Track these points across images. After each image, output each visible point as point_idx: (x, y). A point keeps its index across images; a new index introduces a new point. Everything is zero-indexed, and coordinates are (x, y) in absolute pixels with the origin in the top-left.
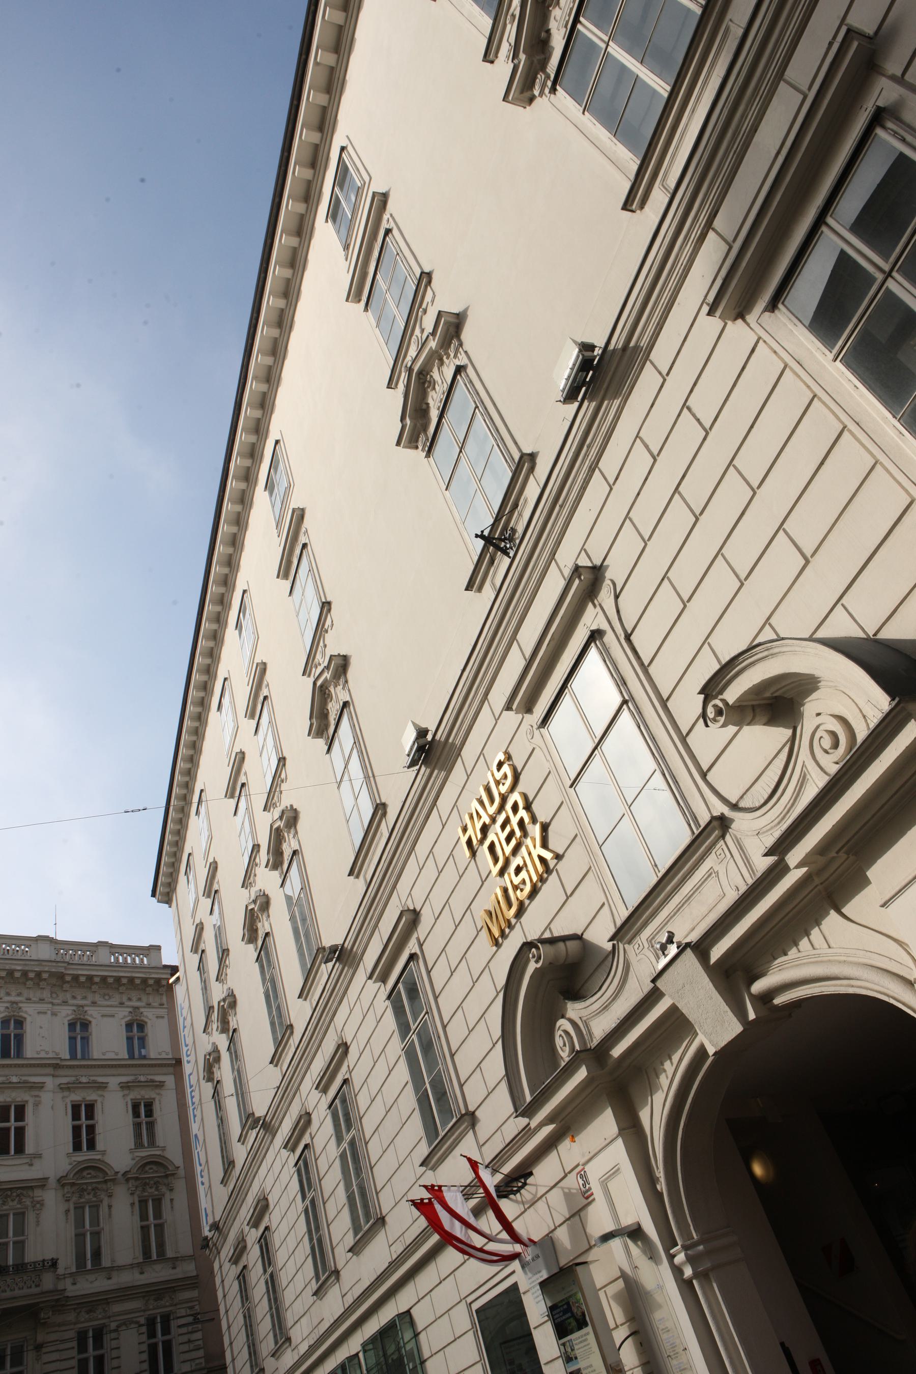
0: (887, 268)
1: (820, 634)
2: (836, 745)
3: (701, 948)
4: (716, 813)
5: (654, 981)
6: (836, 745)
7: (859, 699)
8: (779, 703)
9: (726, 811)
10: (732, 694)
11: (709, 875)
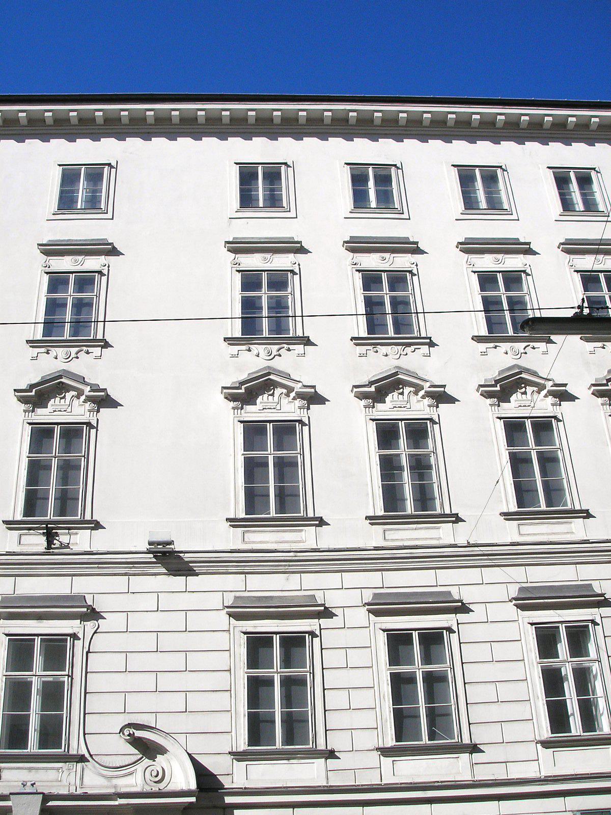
0: (69, 297)
1: (198, 758)
2: (156, 776)
3: (46, 798)
4: (80, 753)
5: (11, 794)
6: (156, 776)
7: (183, 778)
8: (149, 750)
9: (87, 755)
10: (138, 734)
11: (58, 769)
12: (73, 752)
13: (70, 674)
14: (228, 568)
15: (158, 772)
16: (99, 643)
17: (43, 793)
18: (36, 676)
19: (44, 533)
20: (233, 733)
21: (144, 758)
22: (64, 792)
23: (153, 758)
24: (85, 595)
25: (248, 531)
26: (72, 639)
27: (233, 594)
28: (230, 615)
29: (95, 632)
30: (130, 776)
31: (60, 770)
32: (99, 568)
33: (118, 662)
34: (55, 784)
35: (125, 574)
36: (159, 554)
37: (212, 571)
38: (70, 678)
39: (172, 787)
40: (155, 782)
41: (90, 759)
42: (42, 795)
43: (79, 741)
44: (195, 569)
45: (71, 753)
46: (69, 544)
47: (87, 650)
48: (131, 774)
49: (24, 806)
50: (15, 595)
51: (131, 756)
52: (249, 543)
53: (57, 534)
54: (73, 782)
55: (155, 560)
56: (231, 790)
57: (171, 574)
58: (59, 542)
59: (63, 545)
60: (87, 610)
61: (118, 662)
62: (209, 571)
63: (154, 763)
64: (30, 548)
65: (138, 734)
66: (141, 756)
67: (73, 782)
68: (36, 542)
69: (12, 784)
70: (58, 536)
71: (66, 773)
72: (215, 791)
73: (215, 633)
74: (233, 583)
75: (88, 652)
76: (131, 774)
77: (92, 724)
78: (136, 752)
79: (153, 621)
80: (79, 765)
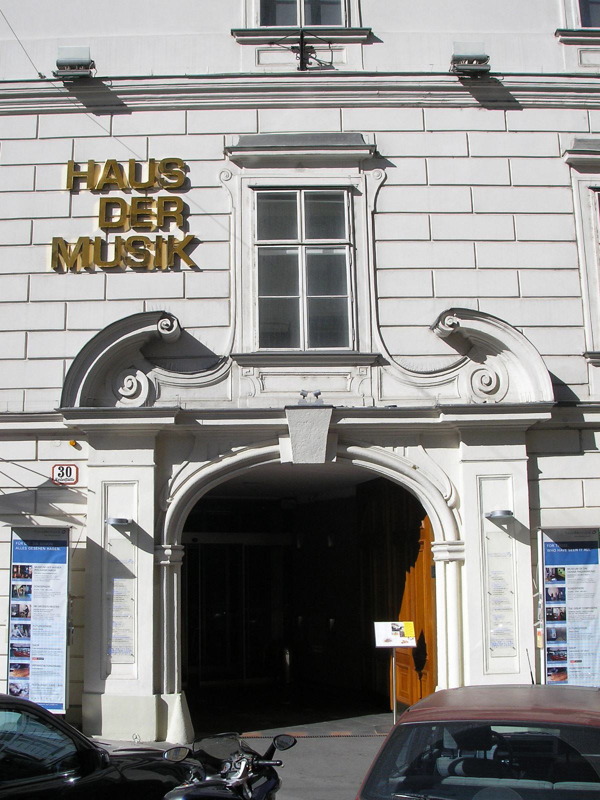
3: (338, 413)
5: (286, 407)
8: (471, 346)
9: (385, 356)
11: (345, 375)
12: (365, 349)
13: (352, 243)
14: (563, 100)
15: (490, 378)
16: (389, 199)
17: (331, 407)
18: (302, 245)
19: (293, 48)
20: (587, 328)
21: (469, 359)
22: (358, 405)
23: (481, 359)
24: (362, 133)
25: (586, 50)
26: (350, 194)
27: (573, 136)
28: (571, 164)
29: (382, 185)
30: (451, 384)
31: (349, 377)
32: (379, 95)
33: (417, 227)
34: (342, 394)
35: (417, 105)
36: (466, 77)
37: (541, 103)
38: (352, 248)
39: (510, 400)
40: (488, 393)
41: (389, 360)
42: (331, 410)
43: (371, 335)
44: (517, 99)
45: (361, 351)
46: (331, 63)
47: (373, 209)
48: (451, 381)
49: (306, 424)
50: (259, 134)
51: (444, 358)
52: (589, 66)
53: (312, 50)
54: (368, 393)
55: (462, 85)
56: (588, 405)
57: (483, 106)
58: (316, 60)
59: (323, 65)
60: (370, 153)
61: (417, 227)
62: (537, 103)
63: (482, 366)
64: (274, 68)
65: (465, 324)
66: (460, 358)
67: (368, 393)
68: (284, 60)
69: (282, 395)
70: (314, 53)
71: (357, 380)
72: (574, 406)
73: (552, 189)
74: (572, 120)
75: (374, 213)
76: (451, 381)
77: (389, 312)
78: (455, 352)
79: (465, 171)
80: (375, 369)
